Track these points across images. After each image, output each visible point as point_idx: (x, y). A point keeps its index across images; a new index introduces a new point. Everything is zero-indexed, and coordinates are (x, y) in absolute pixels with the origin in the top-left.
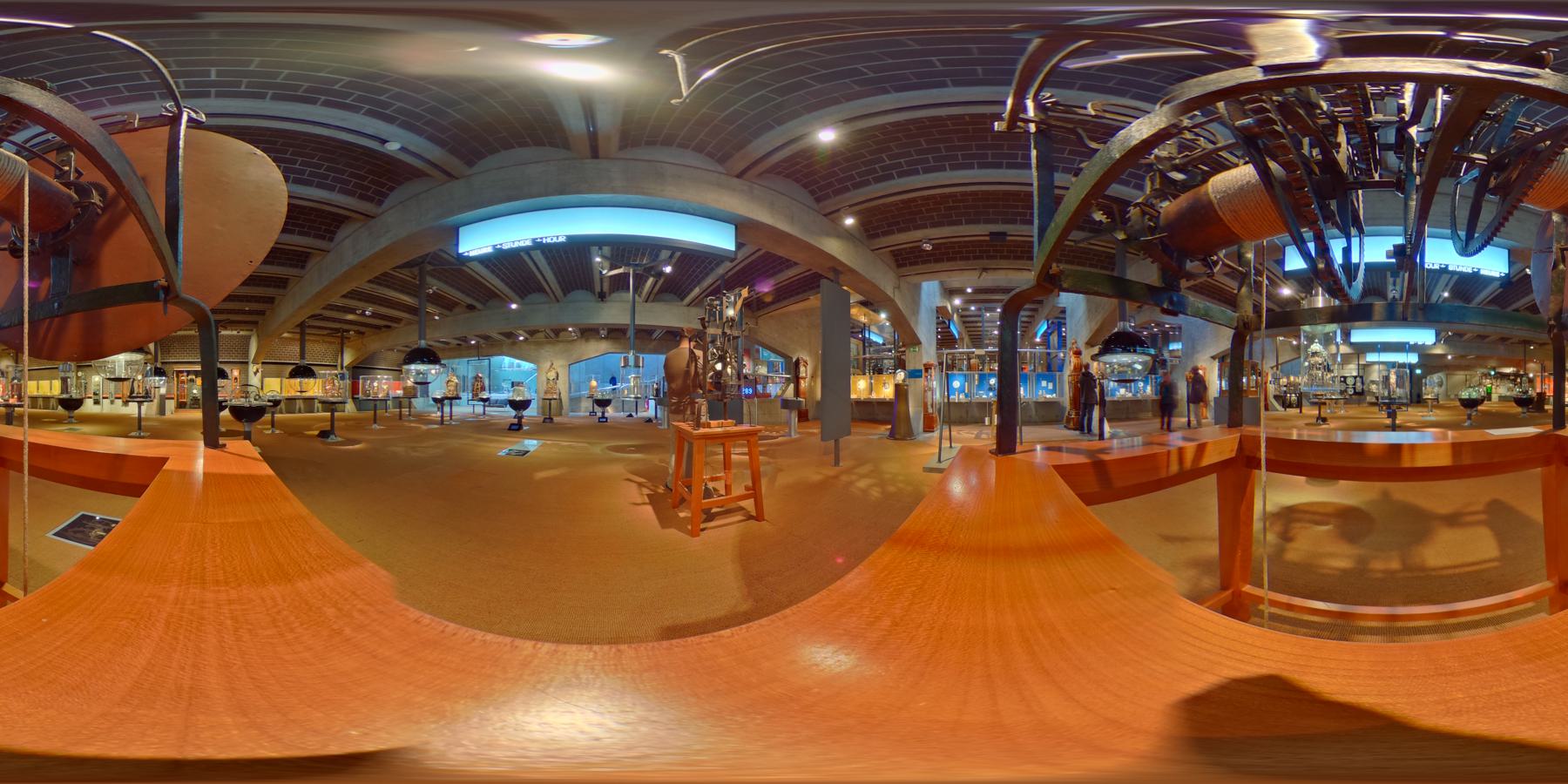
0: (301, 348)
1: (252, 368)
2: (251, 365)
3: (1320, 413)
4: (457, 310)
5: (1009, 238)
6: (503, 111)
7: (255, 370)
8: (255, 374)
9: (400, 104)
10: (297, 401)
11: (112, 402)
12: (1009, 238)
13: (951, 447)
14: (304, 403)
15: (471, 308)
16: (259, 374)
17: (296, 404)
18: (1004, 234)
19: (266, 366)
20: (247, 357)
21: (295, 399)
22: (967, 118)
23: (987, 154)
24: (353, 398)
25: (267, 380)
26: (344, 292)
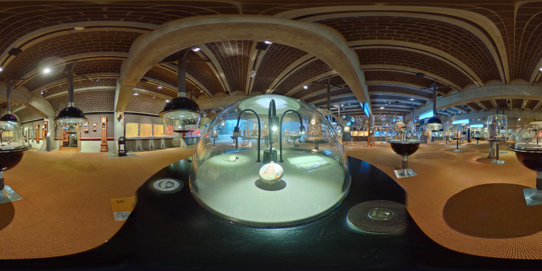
0: (258, 120)
1: (117, 115)
2: (116, 113)
3: (515, 126)
4: (481, 111)
5: (424, 77)
6: (227, 53)
7: (118, 116)
8: (119, 119)
9: (457, 45)
10: (150, 141)
11: (33, 141)
12: (424, 77)
13: (347, 143)
14: (154, 142)
15: (485, 110)
16: (122, 120)
17: (149, 143)
18: (424, 74)
19: (127, 115)
20: (113, 108)
21: (148, 140)
22: (98, 61)
23: (381, 61)
24: (184, 138)
25: (129, 125)
26: (457, 105)
